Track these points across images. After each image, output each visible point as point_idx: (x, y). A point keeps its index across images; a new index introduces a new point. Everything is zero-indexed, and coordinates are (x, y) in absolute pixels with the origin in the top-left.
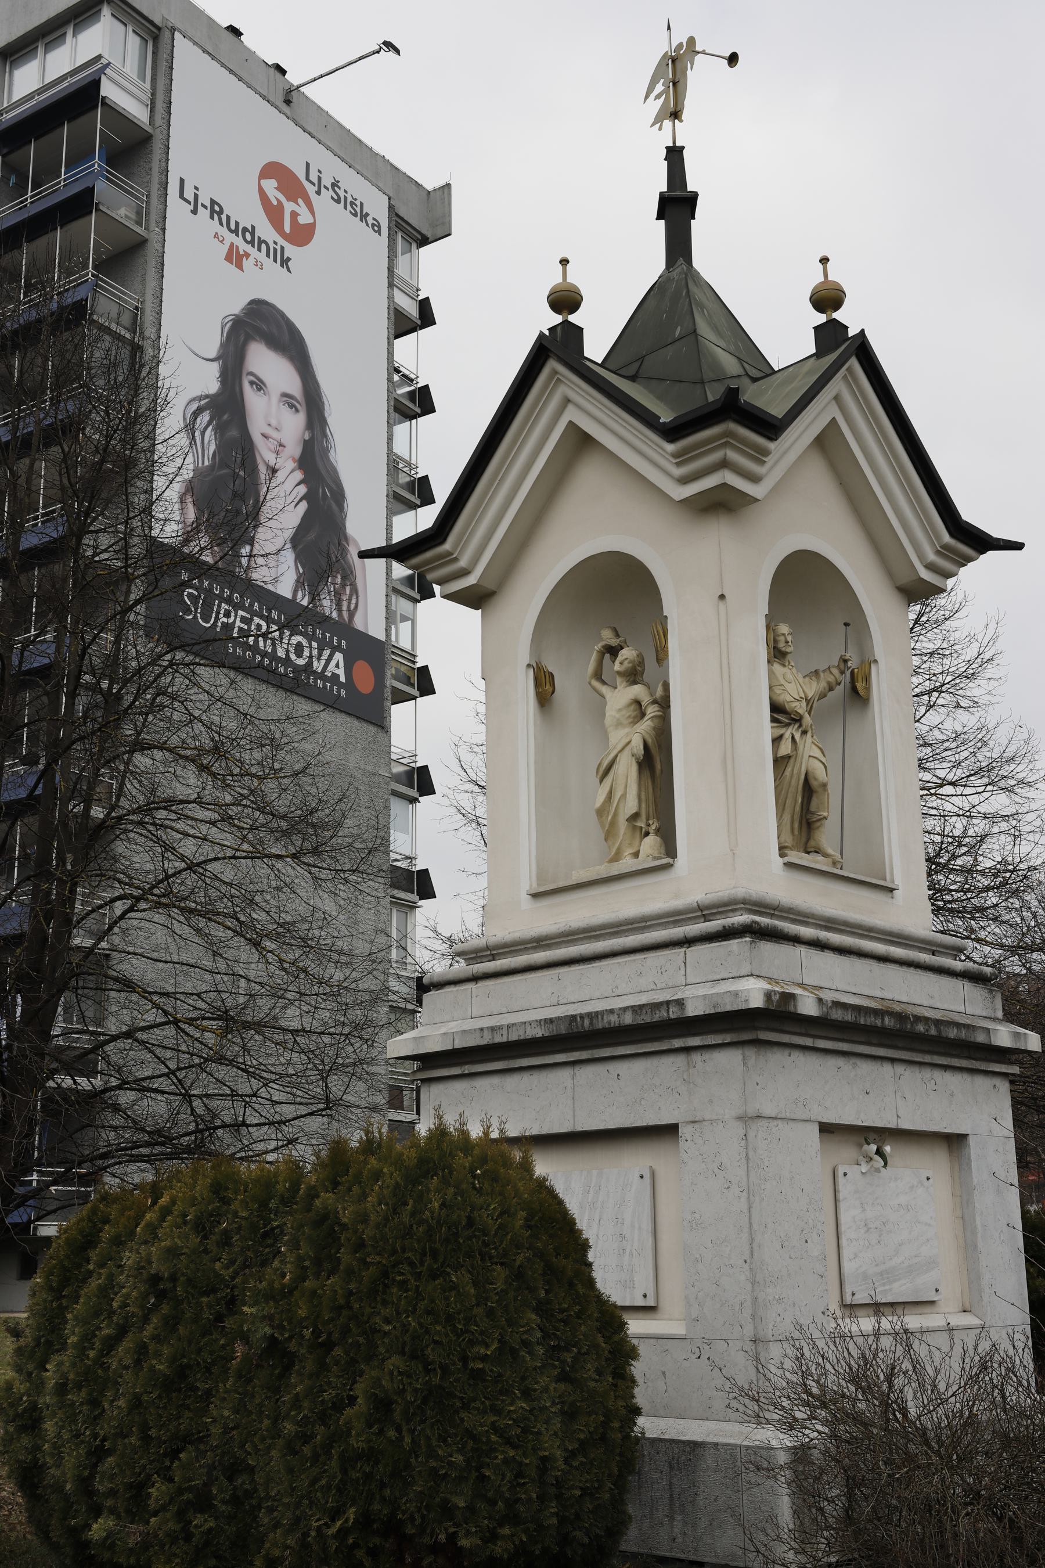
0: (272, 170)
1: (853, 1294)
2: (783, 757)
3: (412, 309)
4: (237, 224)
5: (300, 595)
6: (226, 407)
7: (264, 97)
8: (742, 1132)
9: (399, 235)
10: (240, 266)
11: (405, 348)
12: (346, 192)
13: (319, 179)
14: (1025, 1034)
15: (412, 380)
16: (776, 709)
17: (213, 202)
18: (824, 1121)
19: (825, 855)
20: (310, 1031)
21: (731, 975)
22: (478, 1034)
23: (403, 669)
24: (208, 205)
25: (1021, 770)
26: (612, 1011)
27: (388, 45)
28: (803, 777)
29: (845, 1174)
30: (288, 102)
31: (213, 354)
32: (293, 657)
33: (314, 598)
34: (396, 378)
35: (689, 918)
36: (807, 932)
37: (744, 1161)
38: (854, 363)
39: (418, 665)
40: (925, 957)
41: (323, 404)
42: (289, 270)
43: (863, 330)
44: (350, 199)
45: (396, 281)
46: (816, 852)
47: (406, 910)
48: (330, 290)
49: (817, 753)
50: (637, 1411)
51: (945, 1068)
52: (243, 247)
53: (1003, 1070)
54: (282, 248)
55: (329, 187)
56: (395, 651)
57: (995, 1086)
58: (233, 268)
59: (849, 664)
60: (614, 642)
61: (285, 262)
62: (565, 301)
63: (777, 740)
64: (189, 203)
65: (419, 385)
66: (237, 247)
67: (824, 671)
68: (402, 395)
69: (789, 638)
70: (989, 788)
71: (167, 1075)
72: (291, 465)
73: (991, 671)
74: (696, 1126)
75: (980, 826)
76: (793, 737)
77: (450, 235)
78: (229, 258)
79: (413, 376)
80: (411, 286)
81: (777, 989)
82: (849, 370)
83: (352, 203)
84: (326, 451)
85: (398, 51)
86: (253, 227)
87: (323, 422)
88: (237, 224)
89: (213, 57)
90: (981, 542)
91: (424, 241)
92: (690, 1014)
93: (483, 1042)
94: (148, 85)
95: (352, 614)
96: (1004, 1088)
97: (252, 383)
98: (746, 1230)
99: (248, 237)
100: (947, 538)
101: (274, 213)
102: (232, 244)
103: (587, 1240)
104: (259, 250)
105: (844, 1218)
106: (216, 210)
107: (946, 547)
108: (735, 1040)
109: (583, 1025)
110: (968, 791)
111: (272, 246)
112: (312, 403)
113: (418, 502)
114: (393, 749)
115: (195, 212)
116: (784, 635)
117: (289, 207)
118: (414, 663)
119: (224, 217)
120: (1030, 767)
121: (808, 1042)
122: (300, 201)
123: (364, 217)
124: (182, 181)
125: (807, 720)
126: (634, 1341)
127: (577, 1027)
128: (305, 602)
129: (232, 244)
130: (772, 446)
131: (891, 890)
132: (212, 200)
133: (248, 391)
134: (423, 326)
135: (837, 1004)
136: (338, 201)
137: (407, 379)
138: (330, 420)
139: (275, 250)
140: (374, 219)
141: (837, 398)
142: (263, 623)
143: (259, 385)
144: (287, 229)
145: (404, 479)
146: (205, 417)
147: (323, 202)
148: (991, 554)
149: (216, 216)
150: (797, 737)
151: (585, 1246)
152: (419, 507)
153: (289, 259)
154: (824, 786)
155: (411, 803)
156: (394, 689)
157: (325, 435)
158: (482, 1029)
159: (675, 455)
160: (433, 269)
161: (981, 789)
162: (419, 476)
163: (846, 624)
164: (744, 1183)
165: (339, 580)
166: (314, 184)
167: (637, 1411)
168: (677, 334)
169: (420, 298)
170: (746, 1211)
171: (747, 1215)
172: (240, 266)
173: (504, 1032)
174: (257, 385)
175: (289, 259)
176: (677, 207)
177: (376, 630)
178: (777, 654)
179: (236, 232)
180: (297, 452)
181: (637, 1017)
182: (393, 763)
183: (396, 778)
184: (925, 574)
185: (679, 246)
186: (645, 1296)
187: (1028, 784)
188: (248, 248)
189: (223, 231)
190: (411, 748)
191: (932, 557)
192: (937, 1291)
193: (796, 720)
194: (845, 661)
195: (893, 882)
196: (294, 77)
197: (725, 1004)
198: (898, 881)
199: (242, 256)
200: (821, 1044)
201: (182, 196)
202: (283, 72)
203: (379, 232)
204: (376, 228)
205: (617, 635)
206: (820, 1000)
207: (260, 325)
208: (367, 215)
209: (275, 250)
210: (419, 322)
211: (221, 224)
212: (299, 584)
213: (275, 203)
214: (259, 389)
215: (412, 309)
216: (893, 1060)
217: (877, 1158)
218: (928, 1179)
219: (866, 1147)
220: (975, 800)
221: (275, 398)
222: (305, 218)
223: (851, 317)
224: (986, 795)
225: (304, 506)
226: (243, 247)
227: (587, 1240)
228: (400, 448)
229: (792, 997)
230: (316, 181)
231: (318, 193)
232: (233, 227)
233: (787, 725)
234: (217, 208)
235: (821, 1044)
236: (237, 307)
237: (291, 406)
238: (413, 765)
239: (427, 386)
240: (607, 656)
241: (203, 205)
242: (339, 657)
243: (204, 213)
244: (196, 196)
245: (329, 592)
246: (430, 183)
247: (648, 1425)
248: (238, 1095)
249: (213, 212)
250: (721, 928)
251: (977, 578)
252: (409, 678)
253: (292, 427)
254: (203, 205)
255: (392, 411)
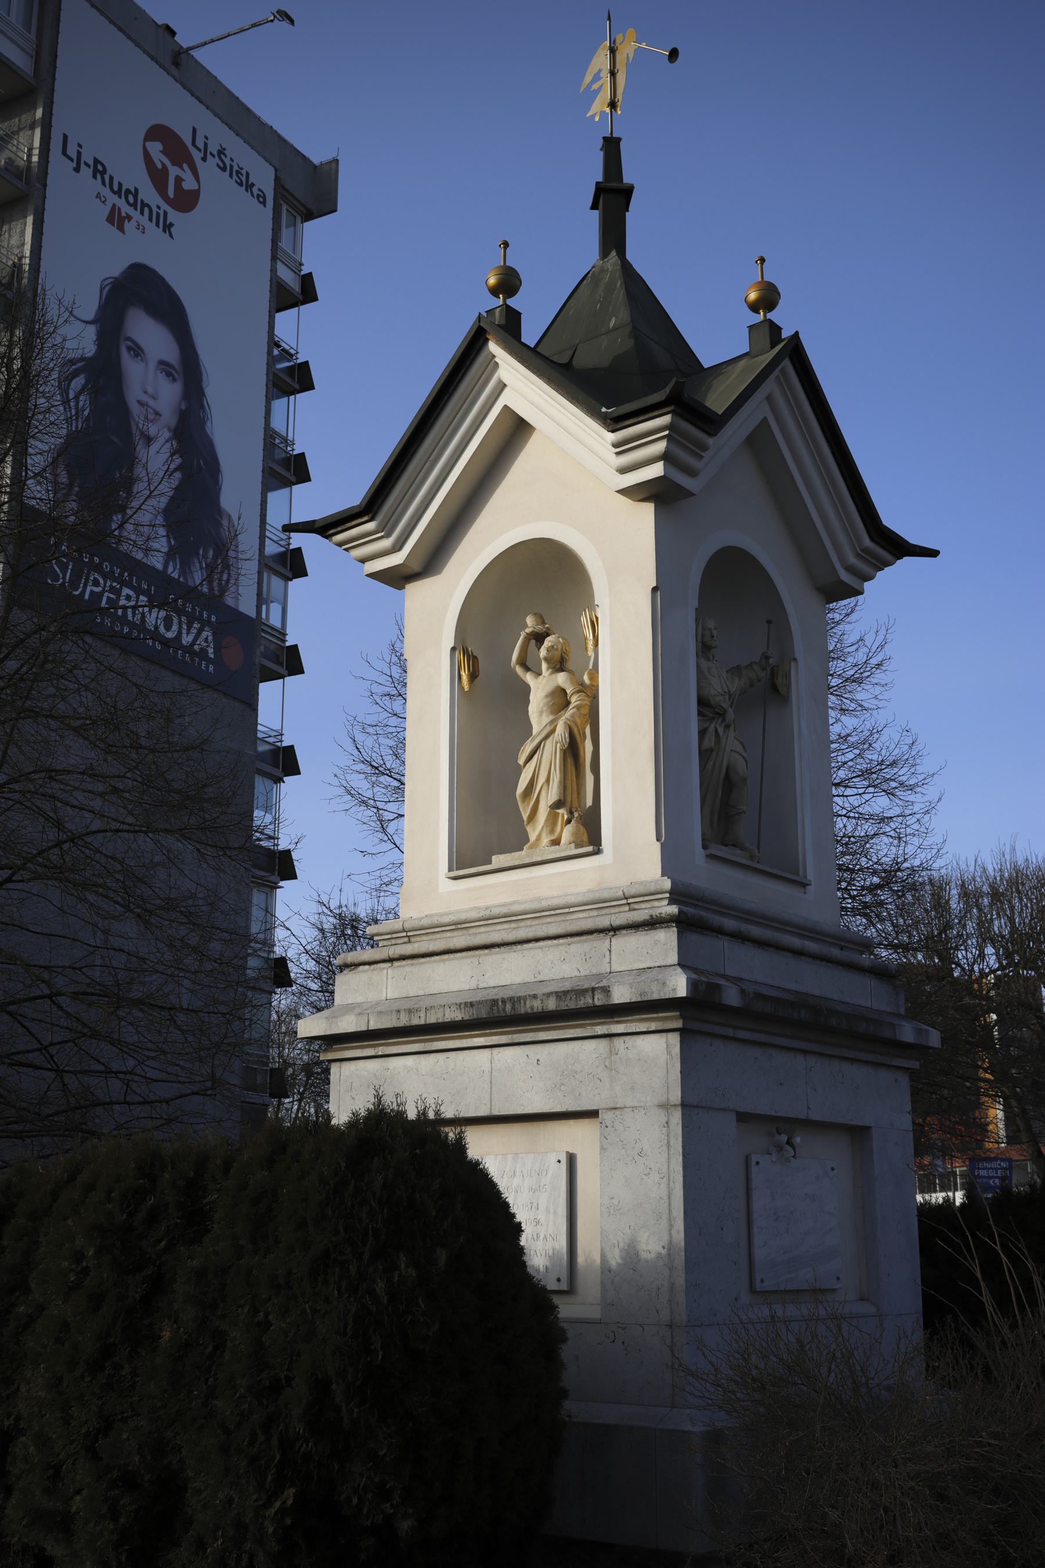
0: (158, 133)
1: (762, 1281)
2: (706, 750)
3: (295, 285)
4: (120, 185)
5: (170, 569)
6: (103, 372)
7: (152, 58)
8: (664, 1119)
9: (285, 207)
10: (121, 229)
11: (286, 322)
12: (232, 160)
13: (206, 145)
14: (927, 1031)
15: (291, 356)
16: (702, 702)
17: (96, 161)
18: (741, 1110)
19: (743, 848)
20: (188, 1010)
21: (657, 964)
22: (394, 1016)
23: (272, 647)
24: (91, 164)
25: (903, 773)
26: (535, 996)
27: (285, 16)
28: (724, 770)
29: (758, 1163)
30: (177, 64)
31: (90, 316)
32: (162, 629)
33: (185, 570)
34: (276, 352)
35: (551, 910)
36: (729, 924)
37: (665, 1148)
38: (787, 363)
39: (288, 644)
40: (835, 952)
41: (201, 374)
42: (171, 236)
43: (797, 333)
44: (235, 168)
45: (280, 254)
46: (734, 845)
47: (267, 890)
48: (211, 256)
49: (739, 748)
50: (563, 1394)
51: (853, 1060)
52: (126, 209)
53: (906, 1065)
54: (165, 213)
55: (215, 153)
56: (265, 628)
57: (896, 1080)
58: (114, 230)
59: (771, 661)
60: (540, 628)
61: (168, 227)
62: (509, 283)
63: (702, 733)
64: (72, 160)
65: (299, 361)
66: (119, 209)
67: (746, 667)
68: (282, 369)
69: (715, 633)
70: (871, 790)
71: (40, 1050)
72: (167, 434)
73: (879, 676)
74: (617, 1112)
75: (868, 828)
76: (716, 731)
77: (335, 211)
78: (110, 219)
79: (292, 352)
80: (295, 261)
81: (703, 979)
82: (783, 371)
83: (238, 172)
84: (203, 422)
85: (292, 22)
86: (136, 190)
87: (201, 394)
88: (120, 185)
89: (102, 13)
90: (899, 548)
91: (309, 216)
92: (616, 1001)
93: (401, 1024)
94: (33, 36)
95: (223, 590)
96: (904, 1081)
97: (129, 349)
98: (665, 1216)
99: (131, 199)
100: (867, 542)
101: (158, 177)
102: (114, 205)
103: (520, 1223)
104: (142, 213)
105: (757, 1205)
106: (99, 169)
107: (865, 550)
108: (659, 1028)
109: (504, 1010)
110: (849, 792)
111: (155, 210)
112: (189, 371)
113: (294, 479)
114: (259, 728)
115: (77, 170)
116: (710, 629)
117: (173, 171)
118: (284, 641)
119: (107, 178)
120: (912, 770)
121: (729, 1032)
122: (185, 166)
123: (249, 187)
124: (65, 137)
125: (731, 714)
126: (565, 1326)
127: (498, 1012)
128: (175, 575)
129: (114, 205)
130: (710, 441)
131: (804, 885)
132: (95, 159)
133: (125, 356)
134: (304, 302)
135: (759, 996)
136: (224, 169)
137: (287, 355)
138: (207, 391)
139: (158, 214)
140: (259, 190)
141: (769, 399)
142: (131, 593)
143: (137, 351)
144: (171, 193)
145: (279, 455)
146: (78, 383)
147: (208, 169)
148: (907, 560)
149: (99, 176)
150: (721, 731)
151: (518, 1229)
152: (295, 484)
153: (171, 225)
154: (745, 780)
155: (275, 783)
156: (263, 667)
157: (202, 406)
158: (398, 1011)
159: (616, 445)
160: (318, 244)
161: (861, 791)
162: (295, 453)
163: (769, 622)
164: (665, 1170)
165: (211, 553)
166: (200, 150)
167: (563, 1394)
168: (612, 324)
169: (303, 273)
170: (665, 1197)
171: (667, 1201)
172: (121, 229)
173: (423, 1015)
174: (134, 351)
175: (171, 225)
176: (613, 198)
177: (247, 606)
178: (705, 649)
179: (118, 193)
180: (173, 423)
181: (562, 1003)
182: (258, 742)
183: (261, 757)
184: (845, 576)
185: (613, 237)
186: (559, 1280)
187: (911, 788)
188: (131, 211)
189: (106, 192)
190: (278, 727)
191: (852, 560)
192: (838, 1279)
193: (720, 714)
194: (767, 658)
195: (805, 877)
196: (183, 39)
197: (652, 993)
198: (811, 876)
199: (124, 218)
200: (741, 1034)
201: (64, 152)
202: (173, 33)
203: (264, 203)
204: (262, 199)
205: (544, 623)
206: (743, 992)
207: (140, 290)
208: (253, 185)
209: (158, 214)
210: (301, 298)
211: (104, 184)
212: (170, 556)
213: (160, 166)
214: (137, 355)
215: (295, 285)
216: (805, 1052)
217: (787, 1147)
218: (833, 1169)
219: (777, 1136)
220: (855, 801)
221: (152, 365)
222: (189, 184)
223: (786, 318)
224: (867, 797)
225: (178, 475)
226: (126, 209)
227: (520, 1223)
228: (278, 423)
229: (718, 987)
230: (202, 147)
231: (204, 159)
232: (116, 188)
233: (712, 719)
234: (100, 168)
235: (741, 1034)
236: (116, 269)
237: (169, 374)
238: (279, 744)
239: (307, 363)
240: (533, 642)
241: (86, 164)
242: (207, 633)
243: (86, 172)
244: (79, 154)
245: (201, 568)
246: (317, 156)
247: (573, 1408)
248: (111, 1072)
249: (95, 171)
250: (647, 917)
251: (890, 586)
252: (278, 657)
253: (168, 395)
254: (86, 164)
255: (271, 385)
